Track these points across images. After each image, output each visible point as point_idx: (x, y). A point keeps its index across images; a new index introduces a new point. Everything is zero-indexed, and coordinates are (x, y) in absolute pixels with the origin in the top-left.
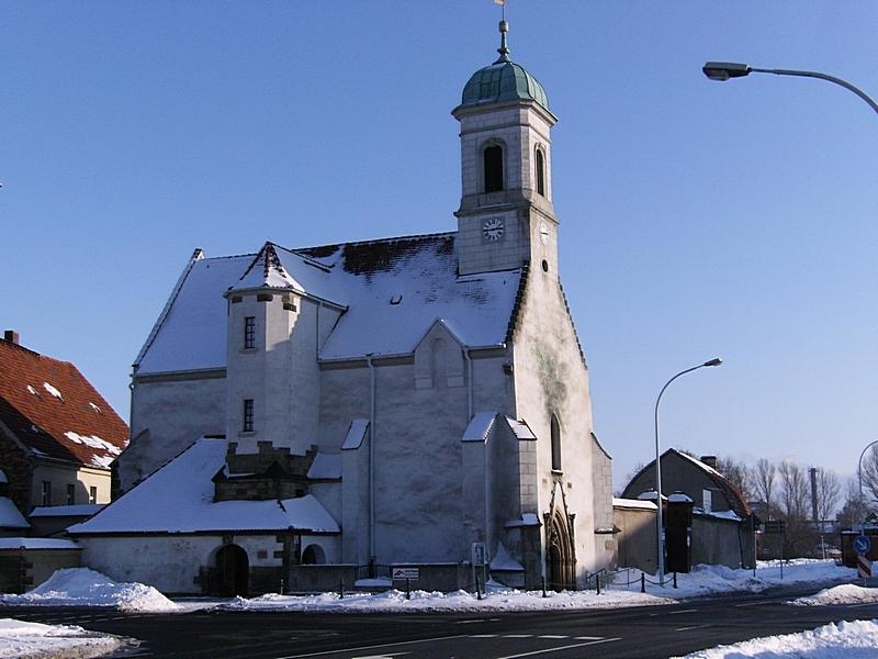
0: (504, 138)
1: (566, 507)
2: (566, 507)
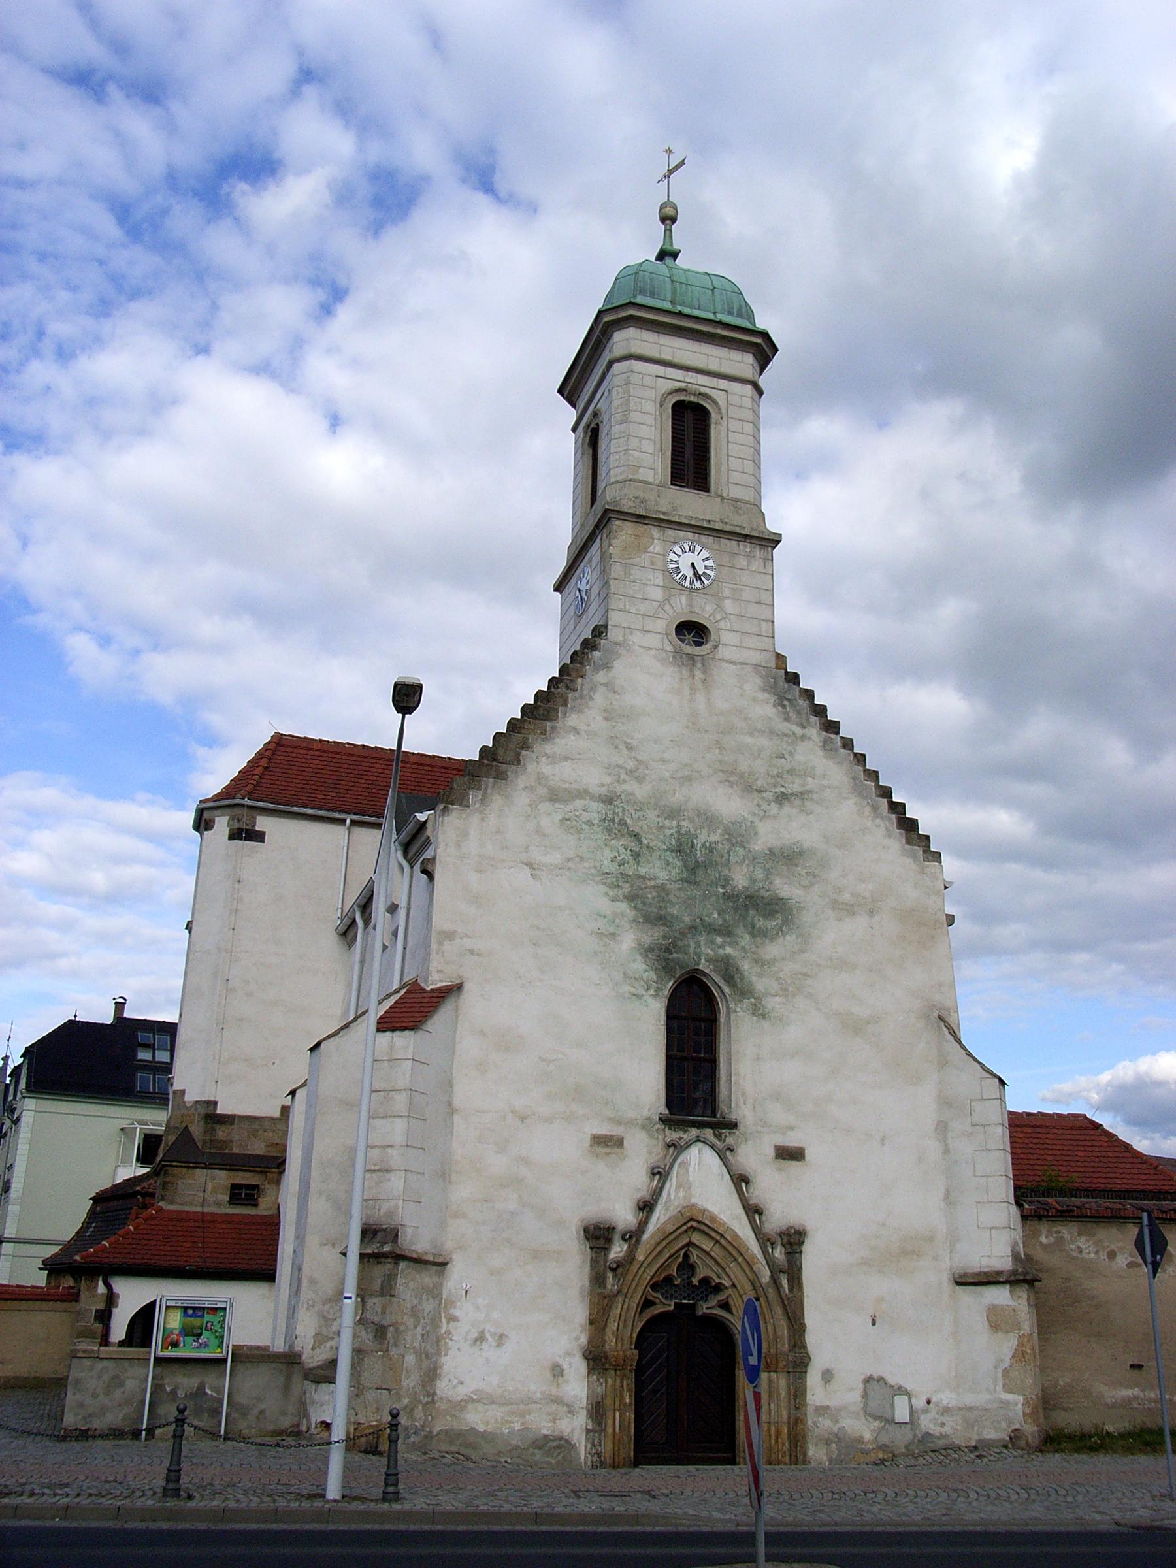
0: (719, 397)
1: (753, 1211)
2: (753, 1211)
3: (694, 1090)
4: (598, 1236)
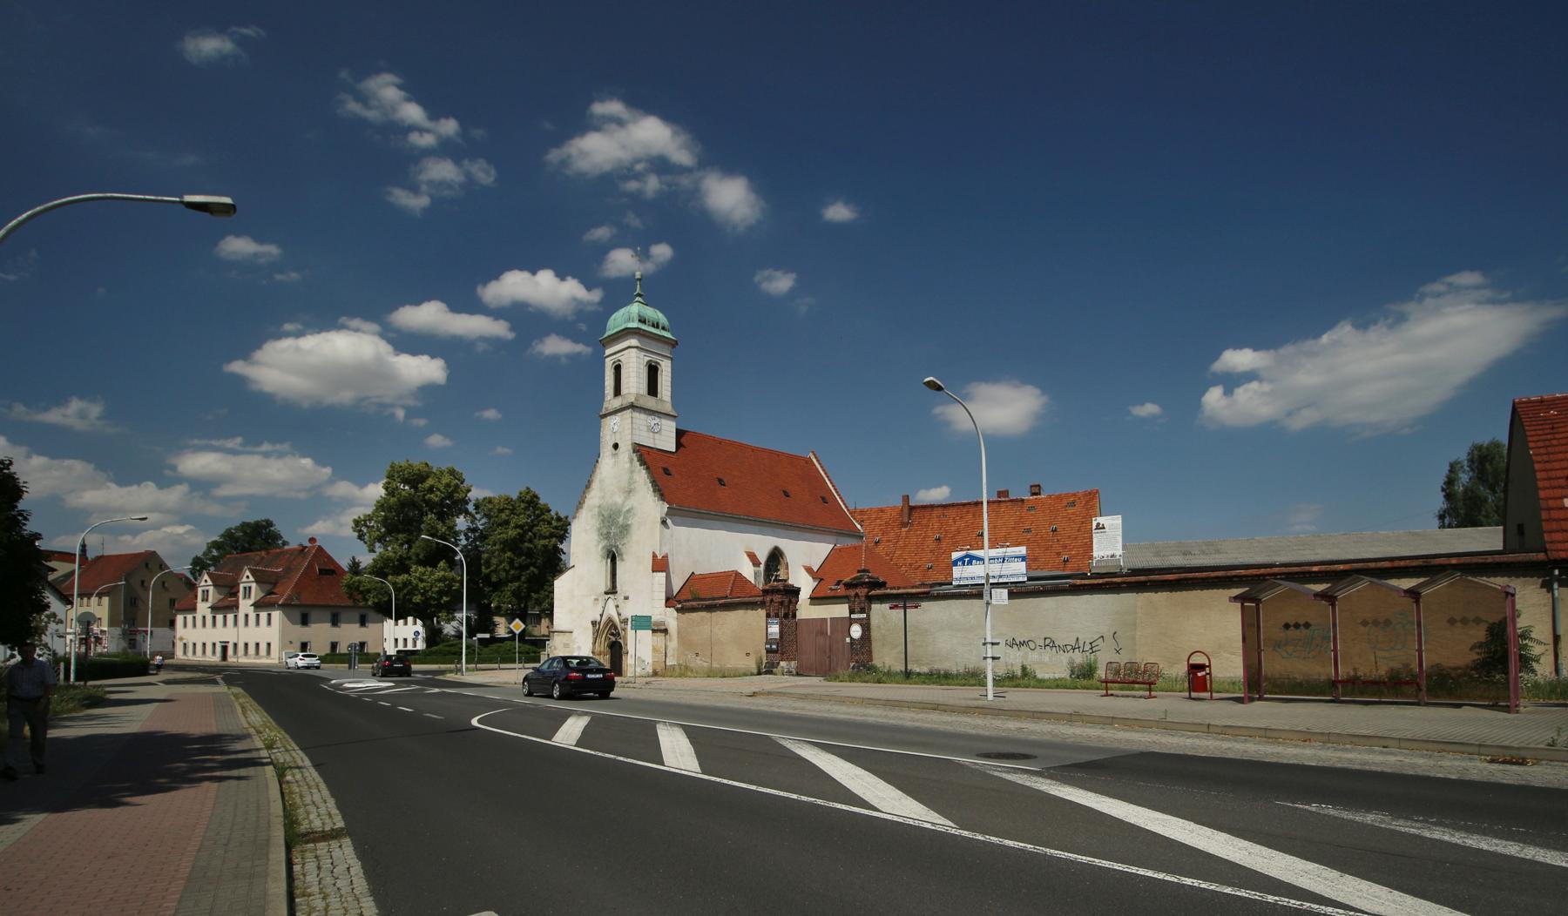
3: (612, 590)
4: (594, 623)
